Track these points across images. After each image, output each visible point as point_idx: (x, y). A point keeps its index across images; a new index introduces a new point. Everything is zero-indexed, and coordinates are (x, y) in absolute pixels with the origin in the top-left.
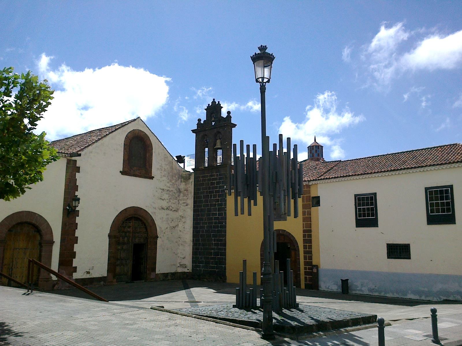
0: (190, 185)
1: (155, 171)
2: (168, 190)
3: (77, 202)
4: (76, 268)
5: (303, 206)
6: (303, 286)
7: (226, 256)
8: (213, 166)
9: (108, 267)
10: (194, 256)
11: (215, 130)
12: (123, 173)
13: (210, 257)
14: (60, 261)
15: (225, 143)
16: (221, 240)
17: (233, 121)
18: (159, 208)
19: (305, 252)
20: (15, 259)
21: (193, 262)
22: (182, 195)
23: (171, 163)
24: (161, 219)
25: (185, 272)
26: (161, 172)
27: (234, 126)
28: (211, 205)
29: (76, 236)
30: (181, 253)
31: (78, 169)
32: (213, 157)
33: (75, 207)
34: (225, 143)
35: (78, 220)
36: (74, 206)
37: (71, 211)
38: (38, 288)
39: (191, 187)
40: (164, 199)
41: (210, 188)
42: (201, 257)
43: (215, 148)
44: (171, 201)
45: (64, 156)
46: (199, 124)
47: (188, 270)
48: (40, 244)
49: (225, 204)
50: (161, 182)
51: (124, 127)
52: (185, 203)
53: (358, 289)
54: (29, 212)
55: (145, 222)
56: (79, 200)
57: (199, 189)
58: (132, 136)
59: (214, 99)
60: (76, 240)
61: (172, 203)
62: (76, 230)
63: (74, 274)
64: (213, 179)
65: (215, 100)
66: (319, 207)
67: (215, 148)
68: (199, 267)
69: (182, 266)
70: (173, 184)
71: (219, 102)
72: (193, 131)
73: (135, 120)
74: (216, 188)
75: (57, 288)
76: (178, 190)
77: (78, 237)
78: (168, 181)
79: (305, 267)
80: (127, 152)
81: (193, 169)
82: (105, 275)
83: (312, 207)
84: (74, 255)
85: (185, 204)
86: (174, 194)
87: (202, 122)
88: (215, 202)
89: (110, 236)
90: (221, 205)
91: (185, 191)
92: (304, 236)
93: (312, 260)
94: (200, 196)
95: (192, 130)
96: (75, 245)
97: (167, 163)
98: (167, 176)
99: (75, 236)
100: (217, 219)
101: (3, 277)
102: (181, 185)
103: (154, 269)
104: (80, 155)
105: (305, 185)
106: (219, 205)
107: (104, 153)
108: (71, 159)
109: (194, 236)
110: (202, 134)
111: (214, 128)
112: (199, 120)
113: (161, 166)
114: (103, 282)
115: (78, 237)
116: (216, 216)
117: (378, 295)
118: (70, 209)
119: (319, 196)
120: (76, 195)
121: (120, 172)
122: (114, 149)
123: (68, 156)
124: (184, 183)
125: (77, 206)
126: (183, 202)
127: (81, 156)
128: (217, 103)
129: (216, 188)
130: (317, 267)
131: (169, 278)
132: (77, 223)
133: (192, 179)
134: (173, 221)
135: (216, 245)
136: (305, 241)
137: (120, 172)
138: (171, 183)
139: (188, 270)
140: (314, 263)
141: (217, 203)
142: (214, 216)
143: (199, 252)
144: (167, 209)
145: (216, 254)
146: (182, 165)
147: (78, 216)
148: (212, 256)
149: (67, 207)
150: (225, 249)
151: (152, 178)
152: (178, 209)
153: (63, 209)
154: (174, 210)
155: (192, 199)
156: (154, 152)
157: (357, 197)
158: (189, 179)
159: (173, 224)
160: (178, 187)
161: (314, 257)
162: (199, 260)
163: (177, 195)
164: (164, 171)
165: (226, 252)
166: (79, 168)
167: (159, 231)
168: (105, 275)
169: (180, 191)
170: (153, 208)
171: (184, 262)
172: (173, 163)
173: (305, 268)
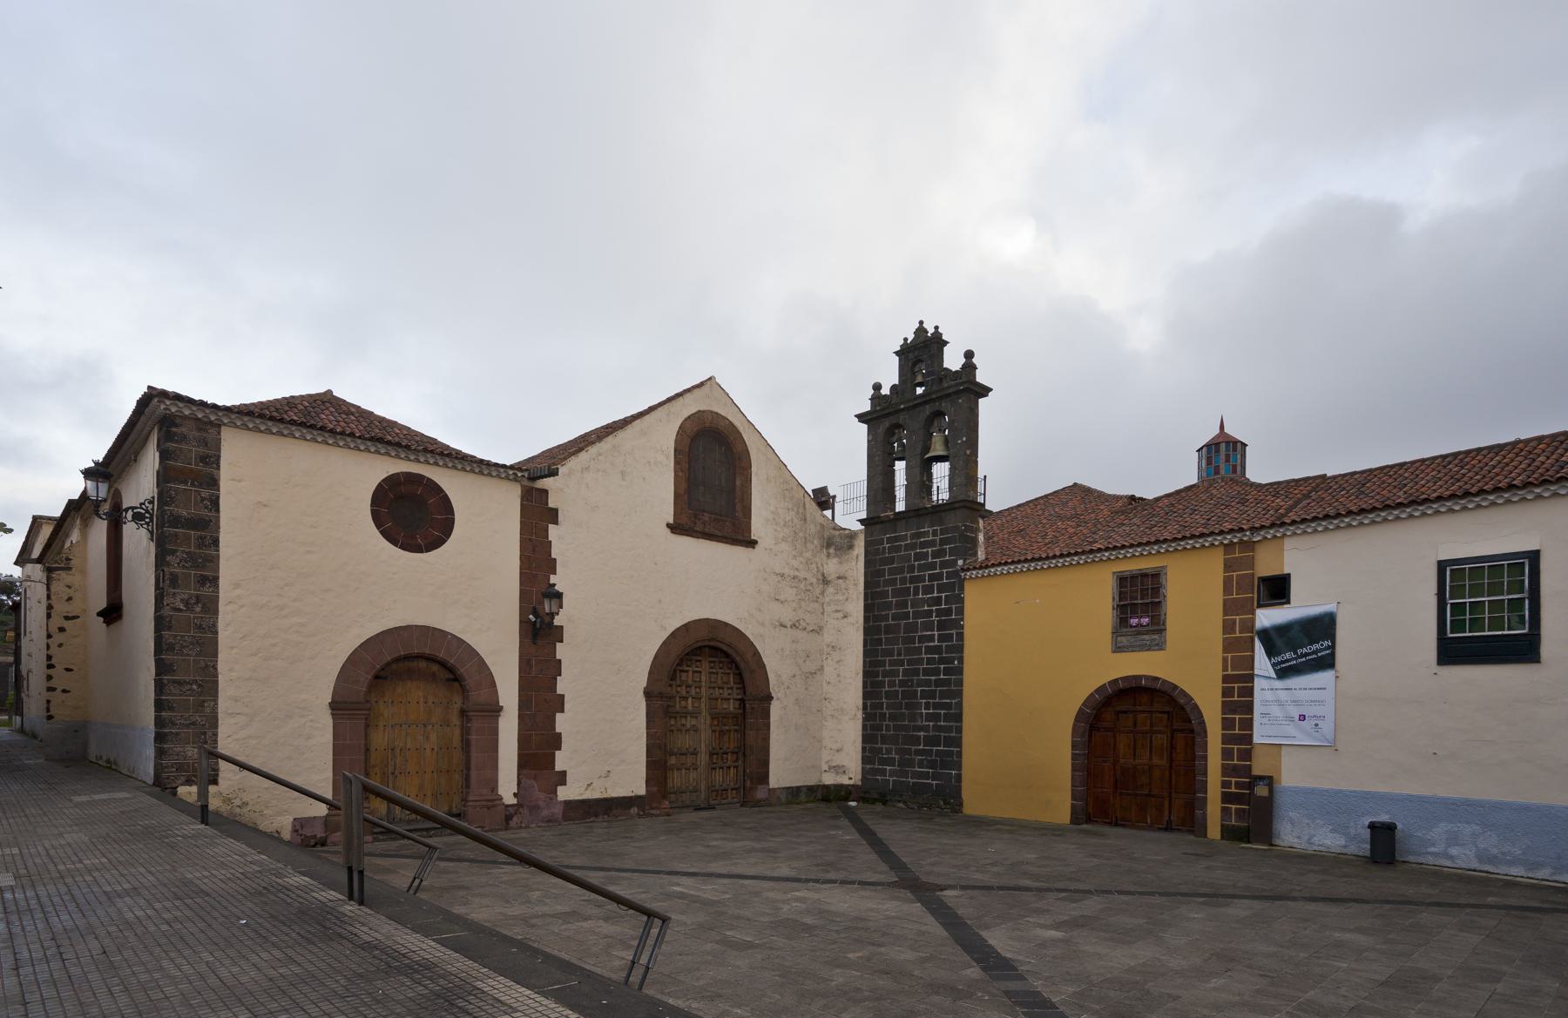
0: (854, 563)
1: (759, 525)
2: (794, 578)
3: (555, 602)
4: (564, 773)
5: (1224, 605)
6: (1214, 831)
7: (961, 747)
8: (922, 510)
10: (868, 746)
11: (928, 409)
12: (675, 528)
14: (520, 756)
15: (959, 442)
17: (981, 377)
18: (772, 624)
20: (398, 751)
21: (865, 760)
22: (830, 590)
23: (802, 505)
24: (777, 652)
25: (842, 786)
26: (776, 530)
28: (917, 615)
29: (559, 692)
30: (831, 737)
31: (553, 516)
32: (921, 483)
33: (552, 615)
34: (959, 442)
35: (561, 651)
36: (547, 614)
37: (540, 628)
39: (855, 566)
40: (786, 601)
42: (886, 748)
43: (926, 456)
44: (803, 604)
45: (511, 478)
46: (877, 398)
47: (851, 779)
48: (463, 713)
49: (961, 611)
50: (776, 555)
51: (674, 402)
52: (839, 611)
53: (1432, 849)
54: (427, 628)
55: (738, 659)
56: (559, 596)
57: (880, 573)
58: (695, 430)
60: (559, 704)
61: (806, 610)
63: (560, 789)
65: (924, 325)
68: (883, 772)
69: (839, 769)
70: (808, 562)
71: (937, 328)
72: (861, 417)
73: (701, 384)
74: (932, 566)
75: (517, 823)
76: (820, 577)
77: (563, 695)
78: (794, 553)
80: (682, 471)
81: (860, 521)
82: (642, 791)
84: (556, 741)
85: (840, 615)
86: (811, 588)
87: (885, 391)
89: (648, 694)
90: (948, 612)
91: (841, 581)
92: (1226, 693)
93: (1250, 761)
94: (884, 590)
95: (856, 416)
97: (790, 506)
98: (790, 540)
101: (372, 797)
102: (827, 564)
104: (554, 473)
105: (1236, 543)
106: (939, 613)
107: (623, 473)
108: (533, 488)
109: (866, 695)
111: (925, 403)
112: (877, 387)
113: (773, 513)
114: (636, 809)
115: (563, 695)
116: (932, 644)
117: (1525, 874)
118: (539, 620)
119: (1286, 572)
120: (551, 582)
121: (668, 525)
122: (649, 462)
123: (523, 476)
124: (835, 560)
125: (558, 614)
126: (835, 608)
129: (932, 566)
130: (1269, 781)
131: (803, 797)
132: (560, 661)
133: (860, 548)
134: (808, 656)
136: (1227, 707)
137: (668, 525)
138: (801, 559)
139: (851, 779)
140: (1256, 771)
141: (934, 608)
142: (927, 644)
143: (882, 736)
144: (794, 626)
146: (828, 513)
147: (562, 642)
148: (920, 745)
149: (531, 617)
150: (959, 730)
151: (752, 544)
152: (821, 628)
153: (521, 622)
154: (812, 631)
155: (858, 599)
156: (756, 475)
157: (1448, 569)
158: (851, 547)
159: (811, 666)
160: (821, 569)
163: (818, 591)
164: (784, 526)
166: (555, 512)
167: (775, 682)
168: (642, 791)
169: (825, 581)
170: (758, 622)
171: (839, 760)
172: (807, 505)
173: (1225, 784)
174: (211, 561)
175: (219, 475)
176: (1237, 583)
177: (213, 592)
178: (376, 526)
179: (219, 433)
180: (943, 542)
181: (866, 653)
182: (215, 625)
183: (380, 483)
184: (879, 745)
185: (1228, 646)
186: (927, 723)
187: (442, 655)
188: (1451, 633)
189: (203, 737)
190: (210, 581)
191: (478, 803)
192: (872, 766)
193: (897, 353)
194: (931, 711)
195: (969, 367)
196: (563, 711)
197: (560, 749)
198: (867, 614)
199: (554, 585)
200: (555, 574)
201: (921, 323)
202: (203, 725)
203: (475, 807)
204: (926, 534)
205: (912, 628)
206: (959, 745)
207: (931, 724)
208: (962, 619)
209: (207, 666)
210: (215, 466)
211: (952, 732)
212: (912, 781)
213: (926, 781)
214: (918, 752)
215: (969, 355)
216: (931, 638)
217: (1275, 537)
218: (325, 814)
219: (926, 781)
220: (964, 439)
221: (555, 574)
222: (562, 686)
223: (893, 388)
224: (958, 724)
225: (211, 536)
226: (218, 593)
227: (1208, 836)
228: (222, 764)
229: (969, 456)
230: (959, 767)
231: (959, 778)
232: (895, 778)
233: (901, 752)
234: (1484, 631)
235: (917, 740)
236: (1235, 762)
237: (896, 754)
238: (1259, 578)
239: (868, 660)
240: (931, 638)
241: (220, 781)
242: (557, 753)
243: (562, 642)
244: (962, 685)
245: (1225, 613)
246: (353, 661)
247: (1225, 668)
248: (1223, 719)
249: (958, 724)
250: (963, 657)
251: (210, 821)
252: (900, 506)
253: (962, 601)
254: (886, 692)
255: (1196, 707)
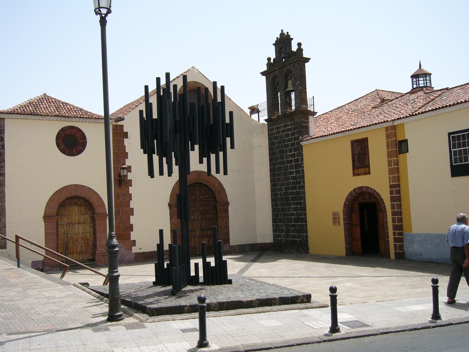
5: (388, 154)
6: (393, 256)
9: (46, 239)
13: (290, 224)
15: (297, 84)
16: (300, 204)
19: (393, 214)
27: (307, 60)
29: (131, 207)
35: (131, 190)
38: (95, 263)
41: (284, 141)
43: (286, 90)
46: (269, 65)
49: (302, 160)
59: (282, 31)
60: (131, 212)
62: (131, 201)
64: (288, 130)
66: (407, 153)
67: (286, 90)
71: (288, 33)
72: (263, 74)
77: (133, 208)
79: (394, 233)
81: (265, 120)
83: (399, 154)
84: (131, 228)
88: (291, 158)
90: (298, 160)
92: (391, 193)
93: (402, 223)
95: (260, 73)
96: (131, 217)
99: (130, 207)
100: (294, 178)
103: (227, 240)
110: (272, 75)
115: (133, 208)
119: (406, 139)
127: (124, 120)
128: (286, 34)
132: (131, 194)
135: (295, 209)
136: (392, 199)
142: (292, 175)
145: (296, 220)
147: (131, 186)
150: (305, 214)
161: (404, 220)
162: (279, 228)
165: (306, 218)
173: (394, 234)
174: (3, 168)
175: (4, 137)
176: (391, 144)
177: (3, 178)
178: (58, 148)
179: (4, 121)
180: (294, 129)
181: (272, 181)
182: (4, 191)
183: (59, 132)
184: (278, 223)
185: (391, 172)
186: (294, 212)
187: (84, 195)
188: (454, 164)
189: (1, 231)
190: (2, 175)
191: (99, 255)
192: (276, 233)
193: (274, 44)
194: (295, 206)
195: (300, 50)
196: (133, 215)
197: (133, 231)
198: (270, 163)
199: (433, 88)
200: (128, 159)
201: (282, 31)
202: (1, 227)
203: (98, 256)
204: (288, 125)
205: (286, 168)
206: (306, 222)
207: (295, 212)
208: (303, 163)
209: (2, 206)
210: (3, 133)
211: (303, 216)
212: (291, 239)
213: (295, 239)
214: (293, 226)
215: (299, 44)
216: (292, 173)
217: (464, 108)
218: (42, 260)
219: (295, 239)
220: (298, 82)
221: (128, 159)
222: (133, 204)
223: (274, 59)
224: (305, 212)
225: (2, 159)
226: (5, 179)
227: (391, 258)
228: (15, 241)
229: (301, 89)
230: (307, 232)
231: (307, 236)
232: (285, 239)
233: (287, 226)
234: (458, 163)
235: (290, 220)
236: (397, 224)
237: (284, 227)
238: (399, 141)
239: (272, 184)
240: (292, 173)
241: (7, 248)
242: (131, 232)
243: (131, 186)
244: (305, 194)
245: (388, 158)
246: (51, 200)
247: (390, 182)
248: (391, 204)
249: (305, 212)
250: (304, 181)
251: (20, 267)
252: (280, 114)
253: (302, 155)
254: (279, 198)
255: (382, 199)
